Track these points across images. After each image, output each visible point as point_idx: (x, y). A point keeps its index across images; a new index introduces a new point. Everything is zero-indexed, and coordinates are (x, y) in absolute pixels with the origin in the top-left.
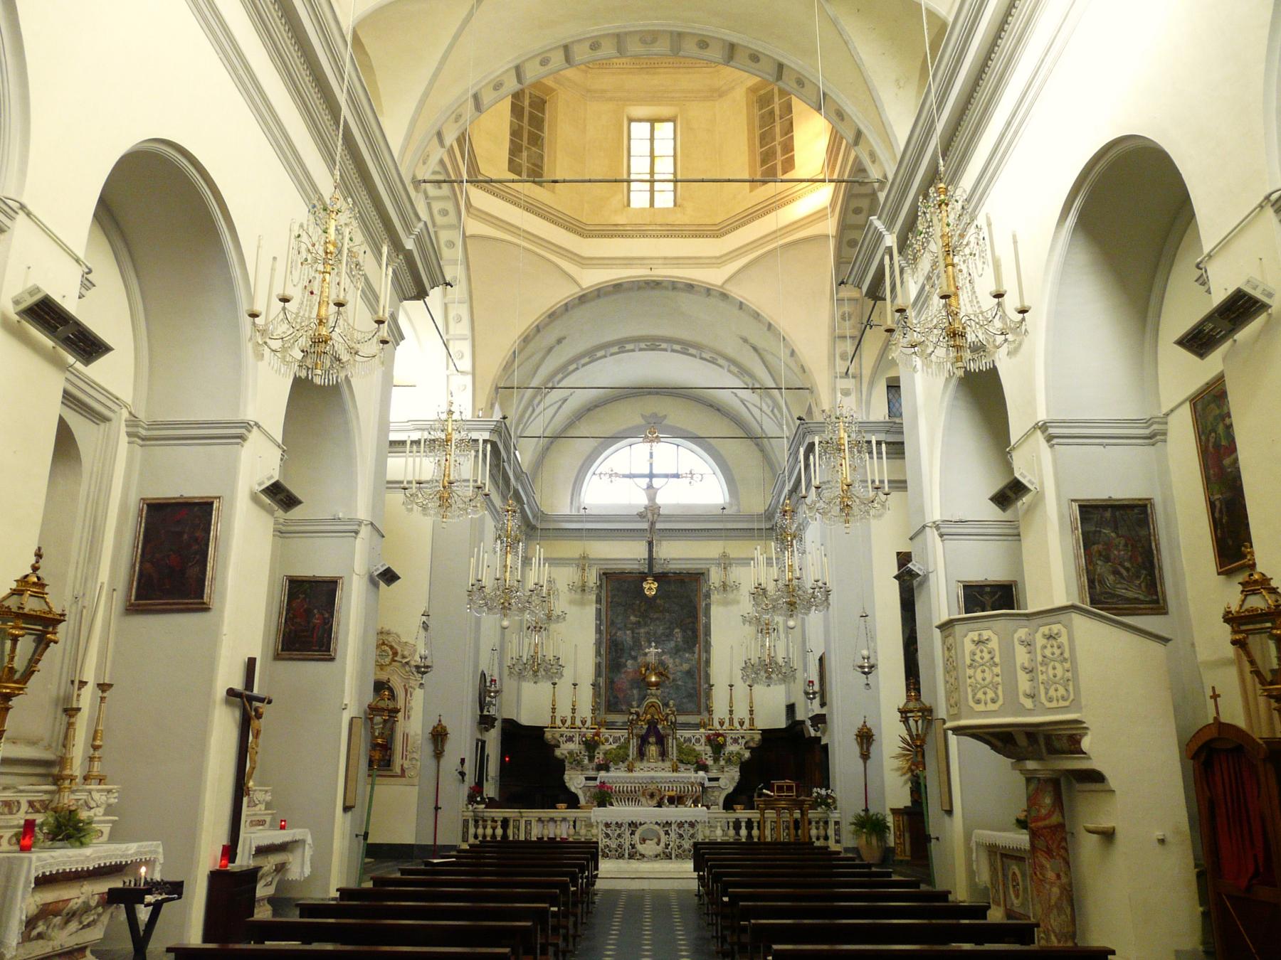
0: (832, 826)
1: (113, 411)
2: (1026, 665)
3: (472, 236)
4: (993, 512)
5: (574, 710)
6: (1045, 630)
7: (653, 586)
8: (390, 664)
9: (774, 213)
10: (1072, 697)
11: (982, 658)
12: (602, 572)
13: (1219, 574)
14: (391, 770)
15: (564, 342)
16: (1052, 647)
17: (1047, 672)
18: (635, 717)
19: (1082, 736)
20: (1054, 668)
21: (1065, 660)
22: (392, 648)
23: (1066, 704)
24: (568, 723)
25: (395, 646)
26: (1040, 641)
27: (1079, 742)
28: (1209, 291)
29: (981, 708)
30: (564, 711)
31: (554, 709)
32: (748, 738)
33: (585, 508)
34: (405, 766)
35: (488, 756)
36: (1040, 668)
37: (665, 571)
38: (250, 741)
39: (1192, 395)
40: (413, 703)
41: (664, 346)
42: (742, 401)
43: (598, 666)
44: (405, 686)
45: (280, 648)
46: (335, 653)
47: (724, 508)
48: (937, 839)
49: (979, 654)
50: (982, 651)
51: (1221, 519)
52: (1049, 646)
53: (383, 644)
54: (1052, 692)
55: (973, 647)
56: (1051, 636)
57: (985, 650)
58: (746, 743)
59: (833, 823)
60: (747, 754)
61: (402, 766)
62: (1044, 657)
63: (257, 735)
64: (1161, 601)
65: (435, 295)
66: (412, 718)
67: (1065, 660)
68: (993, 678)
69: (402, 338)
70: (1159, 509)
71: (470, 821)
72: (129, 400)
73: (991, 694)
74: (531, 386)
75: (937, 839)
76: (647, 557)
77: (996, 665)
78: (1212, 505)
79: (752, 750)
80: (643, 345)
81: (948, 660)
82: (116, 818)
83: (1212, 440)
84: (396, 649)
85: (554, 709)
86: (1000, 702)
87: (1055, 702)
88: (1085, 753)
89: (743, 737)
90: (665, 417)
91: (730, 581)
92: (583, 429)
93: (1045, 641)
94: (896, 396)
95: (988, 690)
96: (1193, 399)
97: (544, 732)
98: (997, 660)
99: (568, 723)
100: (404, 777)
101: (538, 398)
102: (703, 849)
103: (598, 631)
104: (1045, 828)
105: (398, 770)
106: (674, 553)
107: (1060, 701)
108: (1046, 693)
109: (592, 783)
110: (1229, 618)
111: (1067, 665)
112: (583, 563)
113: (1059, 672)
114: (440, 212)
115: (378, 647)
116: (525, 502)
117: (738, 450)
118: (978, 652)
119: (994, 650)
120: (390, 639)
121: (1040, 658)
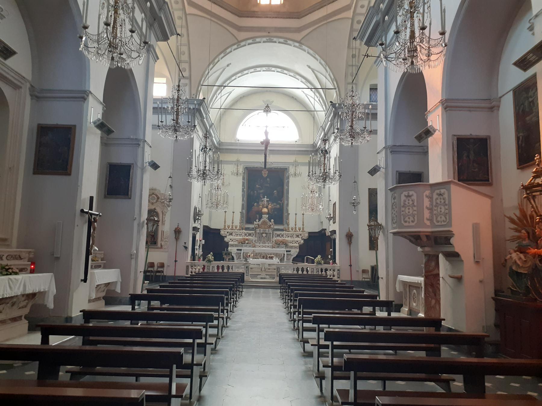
0: (336, 271)
1: (23, 84)
2: (428, 206)
3: (190, 14)
4: (416, 143)
5: (233, 223)
6: (438, 191)
7: (266, 173)
8: (156, 202)
9: (326, 7)
10: (448, 221)
11: (409, 203)
12: (245, 167)
13: (518, 169)
14: (157, 246)
15: (230, 66)
16: (440, 199)
17: (437, 210)
18: (257, 226)
19: (451, 237)
20: (441, 208)
21: (446, 205)
22: (157, 195)
23: (445, 223)
24: (231, 227)
25: (158, 195)
26: (435, 196)
27: (450, 240)
28: (533, 34)
29: (407, 224)
30: (229, 223)
31: (225, 222)
32: (302, 235)
33: (238, 140)
34: (162, 244)
35: (197, 240)
36: (434, 208)
37: (271, 167)
38: (92, 232)
39: (514, 88)
40: (166, 219)
41: (273, 69)
42: (306, 95)
43: (243, 205)
44: (162, 211)
45: (106, 193)
46: (131, 196)
47: (296, 141)
48: (382, 278)
49: (407, 201)
50: (409, 200)
51: (522, 144)
52: (439, 198)
53: (153, 194)
54: (439, 219)
55: (405, 198)
56: (440, 194)
57: (410, 199)
58: (302, 237)
59: (337, 270)
60: (302, 242)
61: (161, 244)
62: (437, 203)
63: (94, 230)
64: (490, 180)
65: (173, 39)
66: (165, 224)
67: (446, 205)
68: (413, 211)
69: (158, 59)
70: (492, 140)
71: (189, 266)
72: (29, 77)
73: (412, 219)
74: (216, 85)
75: (382, 278)
76: (264, 161)
77: (415, 206)
78: (518, 138)
79: (305, 240)
80: (264, 69)
81: (393, 204)
82: (105, 262)
83: (521, 109)
84: (159, 196)
85: (225, 222)
86: (416, 222)
87: (440, 222)
88: (452, 245)
89: (301, 235)
90: (273, 102)
91: (298, 172)
92: (238, 106)
93: (438, 196)
94: (376, 93)
95: (410, 217)
96: (514, 90)
97: (220, 231)
98: (415, 204)
99: (231, 227)
100: (162, 248)
101: (219, 91)
102: (287, 280)
103: (243, 191)
104: (431, 275)
105: (159, 245)
106: (274, 160)
107: (442, 223)
108: (436, 219)
109: (239, 252)
110: (368, 225)
111: (447, 207)
112: (237, 163)
113: (443, 210)
114: (175, 2)
115: (150, 195)
116: (213, 136)
117: (302, 116)
118: (407, 200)
119: (414, 200)
120: (156, 192)
121: (434, 204)
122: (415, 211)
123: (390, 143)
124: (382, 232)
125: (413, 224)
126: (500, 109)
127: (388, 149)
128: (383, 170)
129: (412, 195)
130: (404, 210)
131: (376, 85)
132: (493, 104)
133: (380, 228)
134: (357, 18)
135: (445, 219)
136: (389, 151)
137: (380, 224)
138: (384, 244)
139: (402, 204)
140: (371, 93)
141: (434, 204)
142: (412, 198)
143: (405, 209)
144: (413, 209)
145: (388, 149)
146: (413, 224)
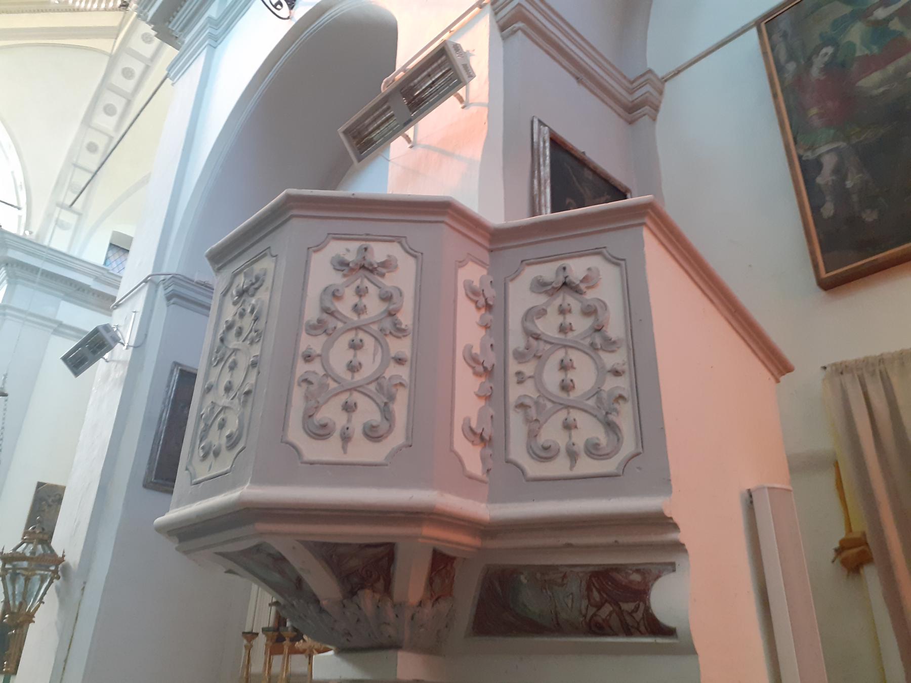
10: (628, 446)
11: (358, 309)
17: (537, 378)
19: (649, 575)
21: (610, 345)
23: (608, 466)
29: (313, 450)
36: (513, 367)
49: (350, 298)
50: (360, 292)
54: (552, 433)
56: (567, 285)
57: (372, 289)
67: (610, 345)
77: (399, 331)
86: (397, 438)
88: (669, 632)
98: (406, 318)
108: (533, 435)
122: (400, 361)
123: (171, 267)
124: (58, 590)
125: (376, 453)
126: (660, 116)
127: (161, 287)
128: (121, 353)
129: (388, 265)
130: (317, 349)
131: (130, 240)
132: (638, 94)
133: (55, 572)
134: (126, 62)
135: (600, 435)
136: (161, 293)
137: (60, 555)
138: (53, 641)
139: (312, 313)
140: (110, 255)
141: (516, 341)
142: (389, 281)
143: (327, 347)
144: (385, 349)
145: (161, 287)
146: (376, 453)
